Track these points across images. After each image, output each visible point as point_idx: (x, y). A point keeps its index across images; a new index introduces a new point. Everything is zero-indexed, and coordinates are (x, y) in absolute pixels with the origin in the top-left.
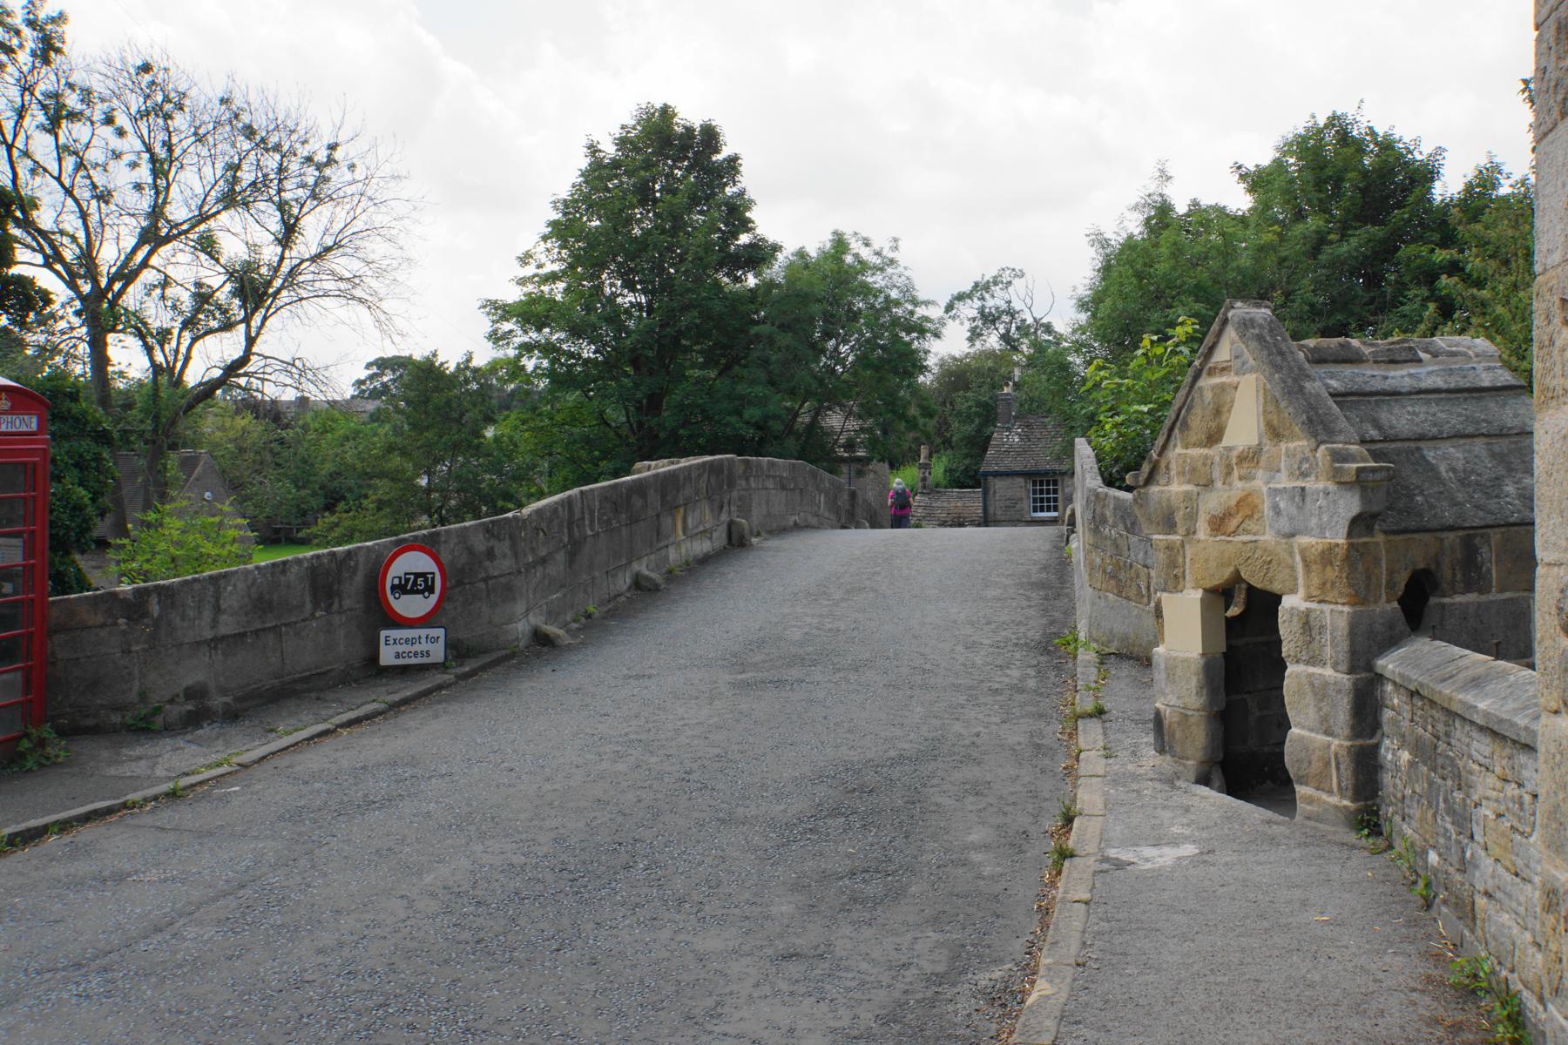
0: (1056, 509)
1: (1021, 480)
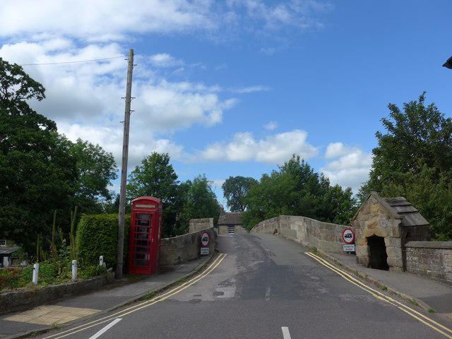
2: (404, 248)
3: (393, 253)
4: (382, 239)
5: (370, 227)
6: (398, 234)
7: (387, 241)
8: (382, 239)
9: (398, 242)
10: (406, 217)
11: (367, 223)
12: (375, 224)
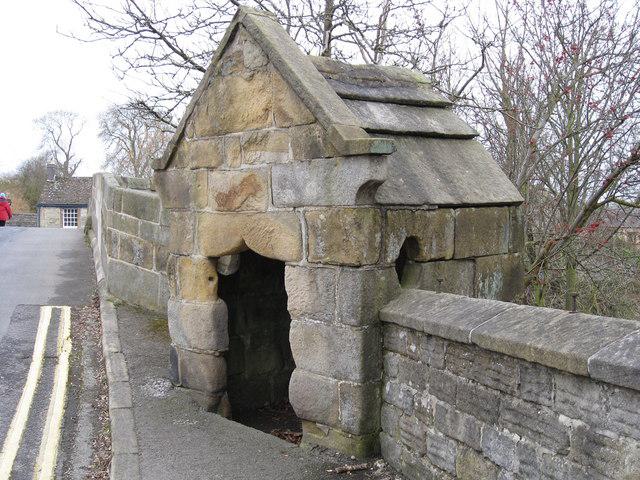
0: (76, 225)
1: (58, 210)
2: (377, 333)
3: (320, 361)
4: (276, 268)
5: (225, 201)
6: (356, 247)
7: (298, 289)
8: (276, 268)
9: (347, 290)
10: (414, 155)
11: (220, 181)
12: (250, 186)
